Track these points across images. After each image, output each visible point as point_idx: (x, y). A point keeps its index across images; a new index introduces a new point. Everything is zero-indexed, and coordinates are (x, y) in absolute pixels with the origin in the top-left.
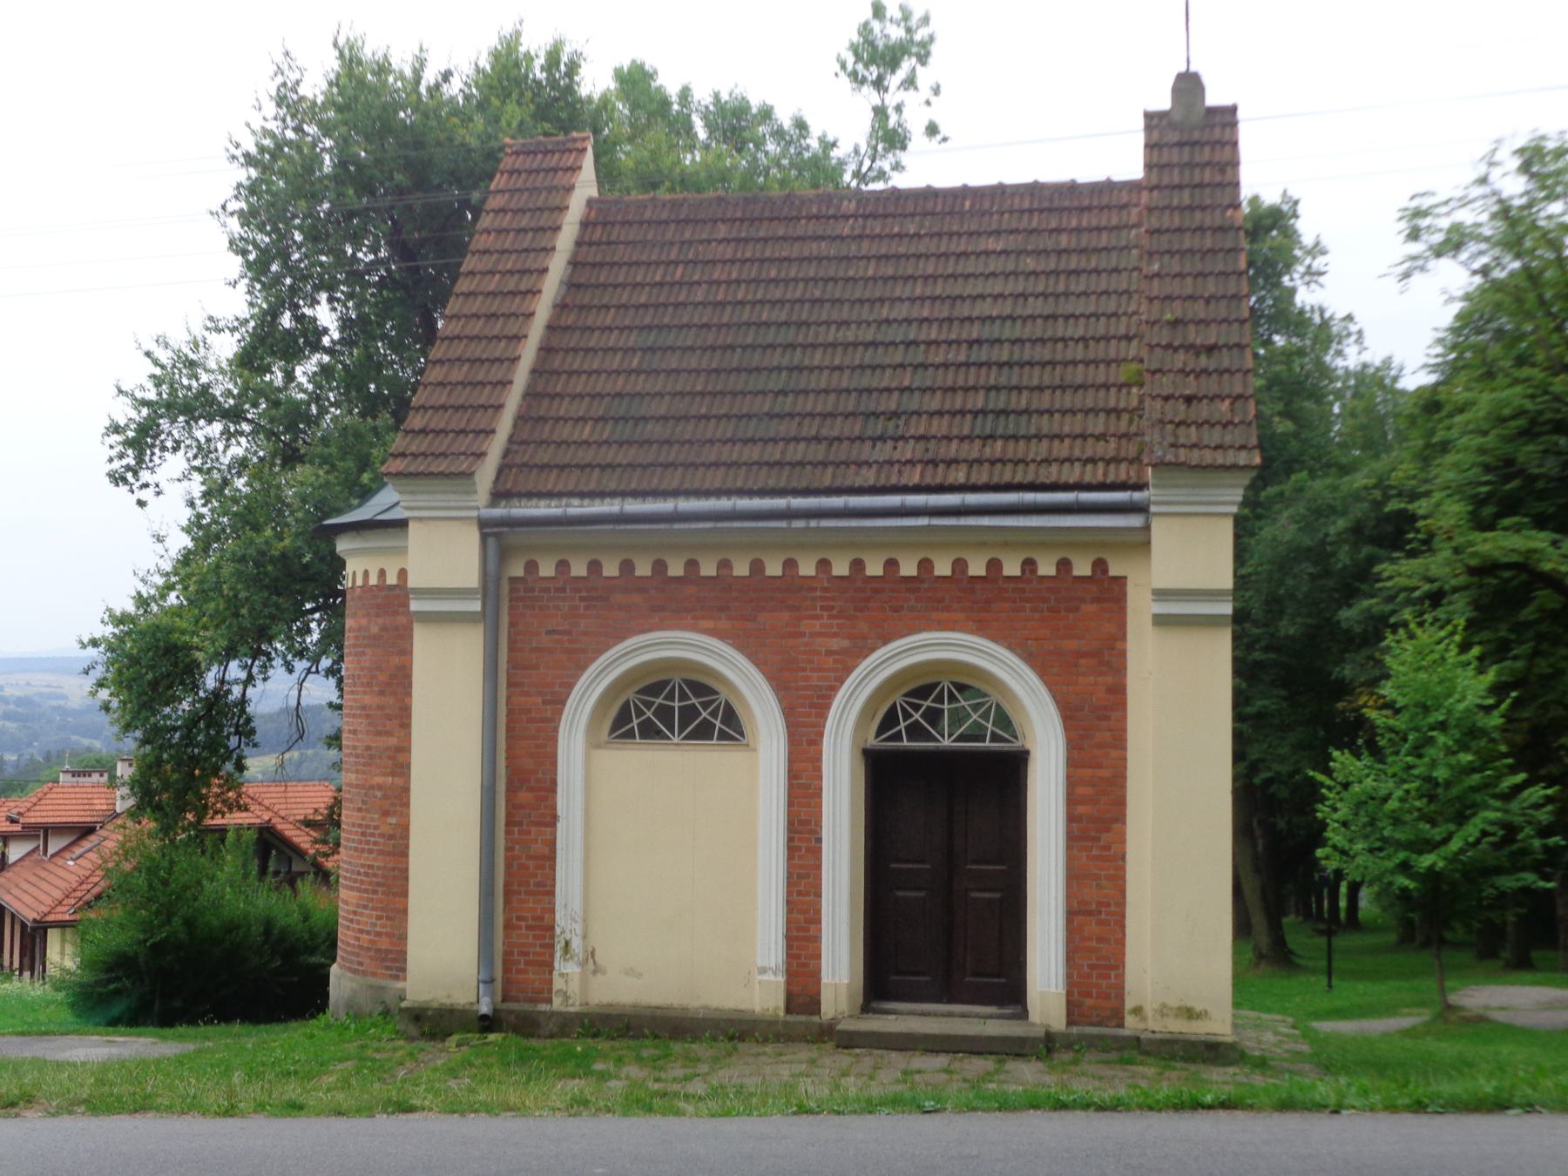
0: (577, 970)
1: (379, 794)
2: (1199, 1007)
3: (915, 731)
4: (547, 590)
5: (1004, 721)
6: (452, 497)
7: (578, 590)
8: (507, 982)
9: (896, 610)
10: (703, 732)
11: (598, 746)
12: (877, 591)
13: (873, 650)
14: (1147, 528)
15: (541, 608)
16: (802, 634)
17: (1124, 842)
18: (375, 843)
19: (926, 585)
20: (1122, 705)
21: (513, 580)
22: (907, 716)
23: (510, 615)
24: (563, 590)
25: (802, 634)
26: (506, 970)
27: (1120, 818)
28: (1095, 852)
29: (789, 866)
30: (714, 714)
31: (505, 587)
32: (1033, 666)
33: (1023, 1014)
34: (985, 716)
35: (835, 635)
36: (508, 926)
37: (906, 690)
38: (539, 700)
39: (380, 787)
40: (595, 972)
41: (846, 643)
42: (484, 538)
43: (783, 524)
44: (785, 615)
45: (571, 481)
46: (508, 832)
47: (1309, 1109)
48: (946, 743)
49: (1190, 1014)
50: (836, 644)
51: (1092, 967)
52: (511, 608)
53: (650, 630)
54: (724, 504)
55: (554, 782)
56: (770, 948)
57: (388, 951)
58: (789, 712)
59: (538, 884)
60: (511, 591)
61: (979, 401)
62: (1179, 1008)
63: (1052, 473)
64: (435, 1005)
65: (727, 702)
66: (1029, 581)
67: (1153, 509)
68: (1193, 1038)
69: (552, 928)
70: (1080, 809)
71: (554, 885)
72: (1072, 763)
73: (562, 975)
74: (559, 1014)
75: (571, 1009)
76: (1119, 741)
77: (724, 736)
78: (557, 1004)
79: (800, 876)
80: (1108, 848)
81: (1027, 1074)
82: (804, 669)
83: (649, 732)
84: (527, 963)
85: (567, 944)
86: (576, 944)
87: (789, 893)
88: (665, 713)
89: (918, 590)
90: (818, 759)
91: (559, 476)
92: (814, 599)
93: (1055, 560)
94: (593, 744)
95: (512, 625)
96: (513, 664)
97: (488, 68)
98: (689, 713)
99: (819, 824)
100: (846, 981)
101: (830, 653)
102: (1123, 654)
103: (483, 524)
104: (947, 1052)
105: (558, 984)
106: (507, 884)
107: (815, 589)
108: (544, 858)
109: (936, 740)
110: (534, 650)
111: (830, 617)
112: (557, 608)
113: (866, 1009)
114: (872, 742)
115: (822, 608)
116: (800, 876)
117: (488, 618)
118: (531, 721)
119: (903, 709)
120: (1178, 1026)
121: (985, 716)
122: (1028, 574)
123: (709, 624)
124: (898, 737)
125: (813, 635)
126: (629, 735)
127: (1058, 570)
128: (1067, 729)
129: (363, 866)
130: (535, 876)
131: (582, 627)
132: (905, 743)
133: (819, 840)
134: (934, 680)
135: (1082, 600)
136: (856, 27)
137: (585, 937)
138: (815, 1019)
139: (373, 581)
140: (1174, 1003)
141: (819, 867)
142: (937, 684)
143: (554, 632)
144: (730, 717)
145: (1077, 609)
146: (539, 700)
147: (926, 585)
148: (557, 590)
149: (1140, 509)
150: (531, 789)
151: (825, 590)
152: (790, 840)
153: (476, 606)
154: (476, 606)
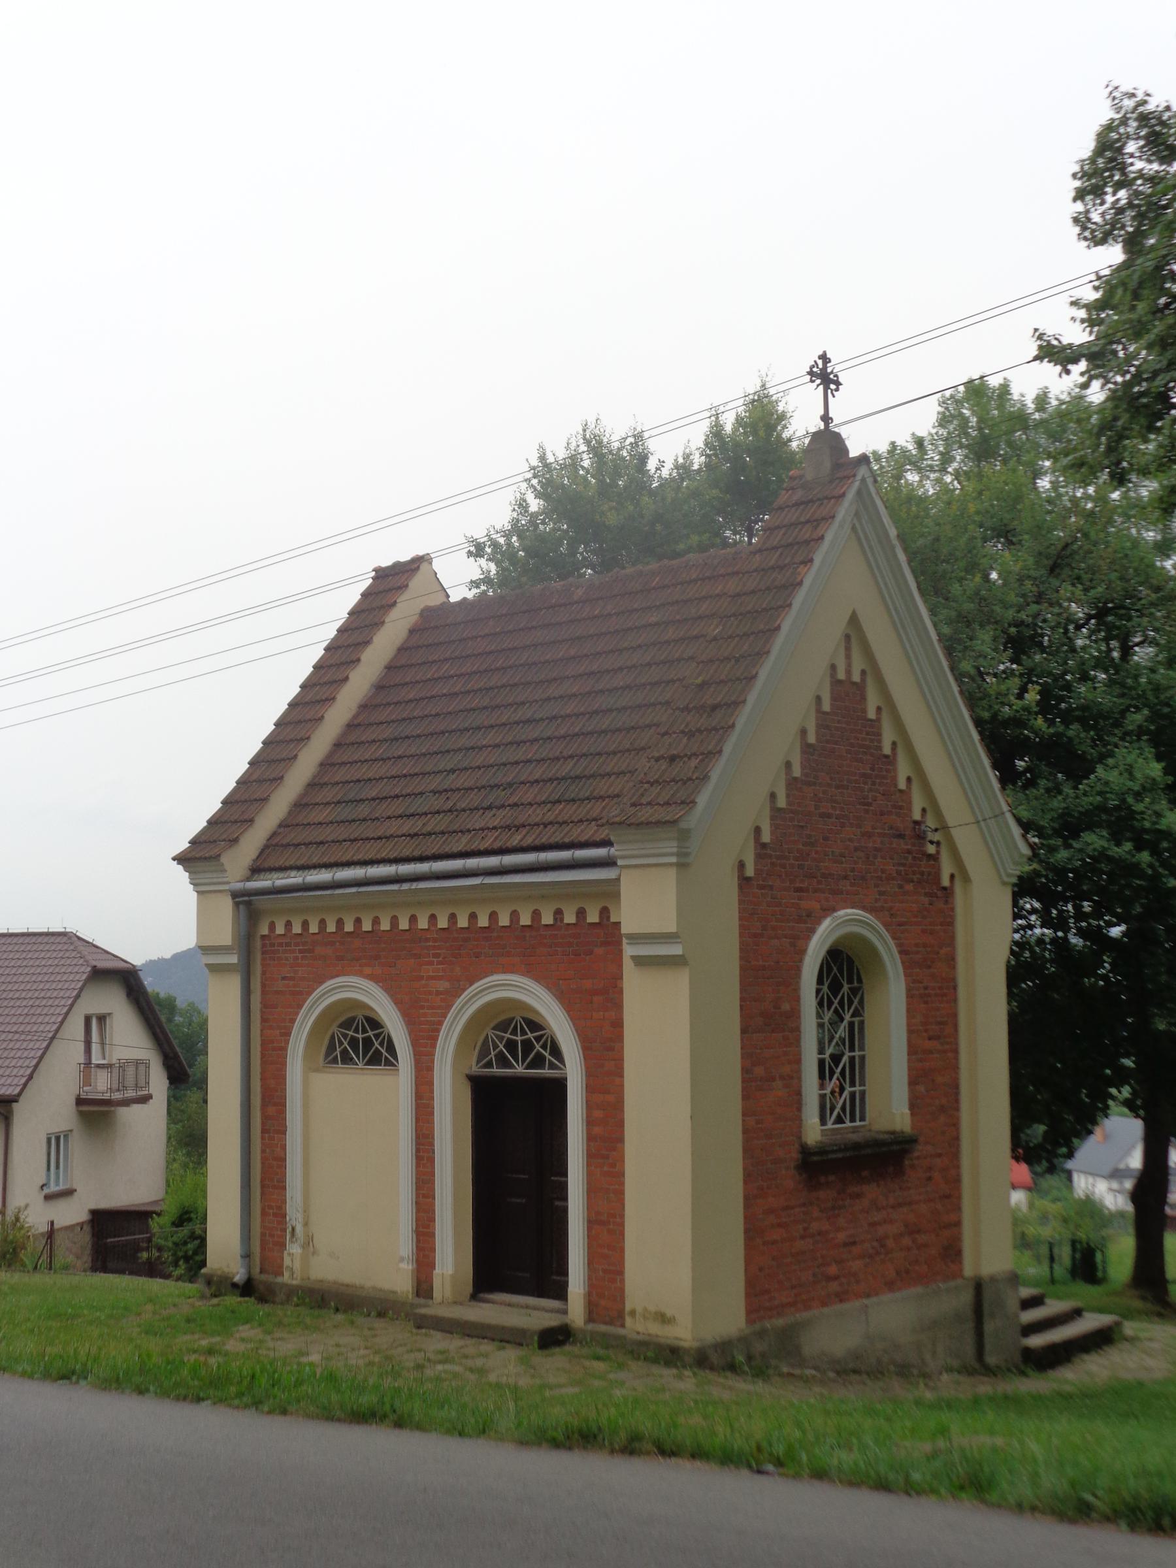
0: (300, 1251)
2: (669, 1313)
4: (281, 945)
6: (215, 875)
8: (263, 1259)
9: (477, 956)
11: (317, 1070)
13: (464, 990)
14: (618, 880)
16: (421, 978)
19: (495, 934)
20: (620, 1037)
21: (263, 937)
22: (538, 1039)
23: (262, 964)
25: (421, 978)
26: (263, 1248)
27: (621, 1140)
28: (606, 1169)
29: (417, 1172)
30: (523, 1033)
31: (258, 943)
35: (440, 978)
36: (264, 1213)
37: (492, 1025)
38: (278, 1032)
40: (314, 1253)
42: (237, 905)
43: (395, 887)
46: (263, 1138)
49: (663, 1318)
50: (443, 985)
51: (605, 1271)
52: (263, 959)
53: (337, 976)
54: (358, 872)
60: (264, 946)
62: (656, 1313)
63: (576, 834)
64: (219, 1273)
67: (620, 862)
68: (662, 1341)
69: (284, 1216)
70: (597, 1130)
73: (289, 1254)
74: (286, 1285)
75: (294, 1282)
78: (286, 1278)
83: (346, 1059)
85: (293, 1229)
86: (299, 1229)
87: (417, 1196)
90: (431, 1084)
91: (316, 849)
93: (599, 907)
94: (310, 1067)
95: (264, 973)
96: (265, 1005)
97: (728, 428)
100: (450, 1272)
101: (438, 993)
103: (235, 895)
104: (478, 1337)
105: (287, 1261)
106: (262, 1180)
107: (427, 940)
109: (514, 1067)
111: (439, 963)
112: (287, 959)
113: (474, 1297)
114: (476, 1070)
117: (620, 936)
120: (655, 1329)
122: (559, 923)
123: (368, 970)
124: (489, 1065)
126: (335, 1061)
127: (577, 917)
132: (495, 1070)
134: (512, 1016)
137: (306, 1224)
140: (652, 1308)
141: (433, 1175)
142: (334, 1033)
145: (591, 952)
146: (278, 1032)
147: (495, 934)
149: (609, 863)
151: (435, 940)
152: (418, 1150)
153: (233, 959)
154: (233, 959)
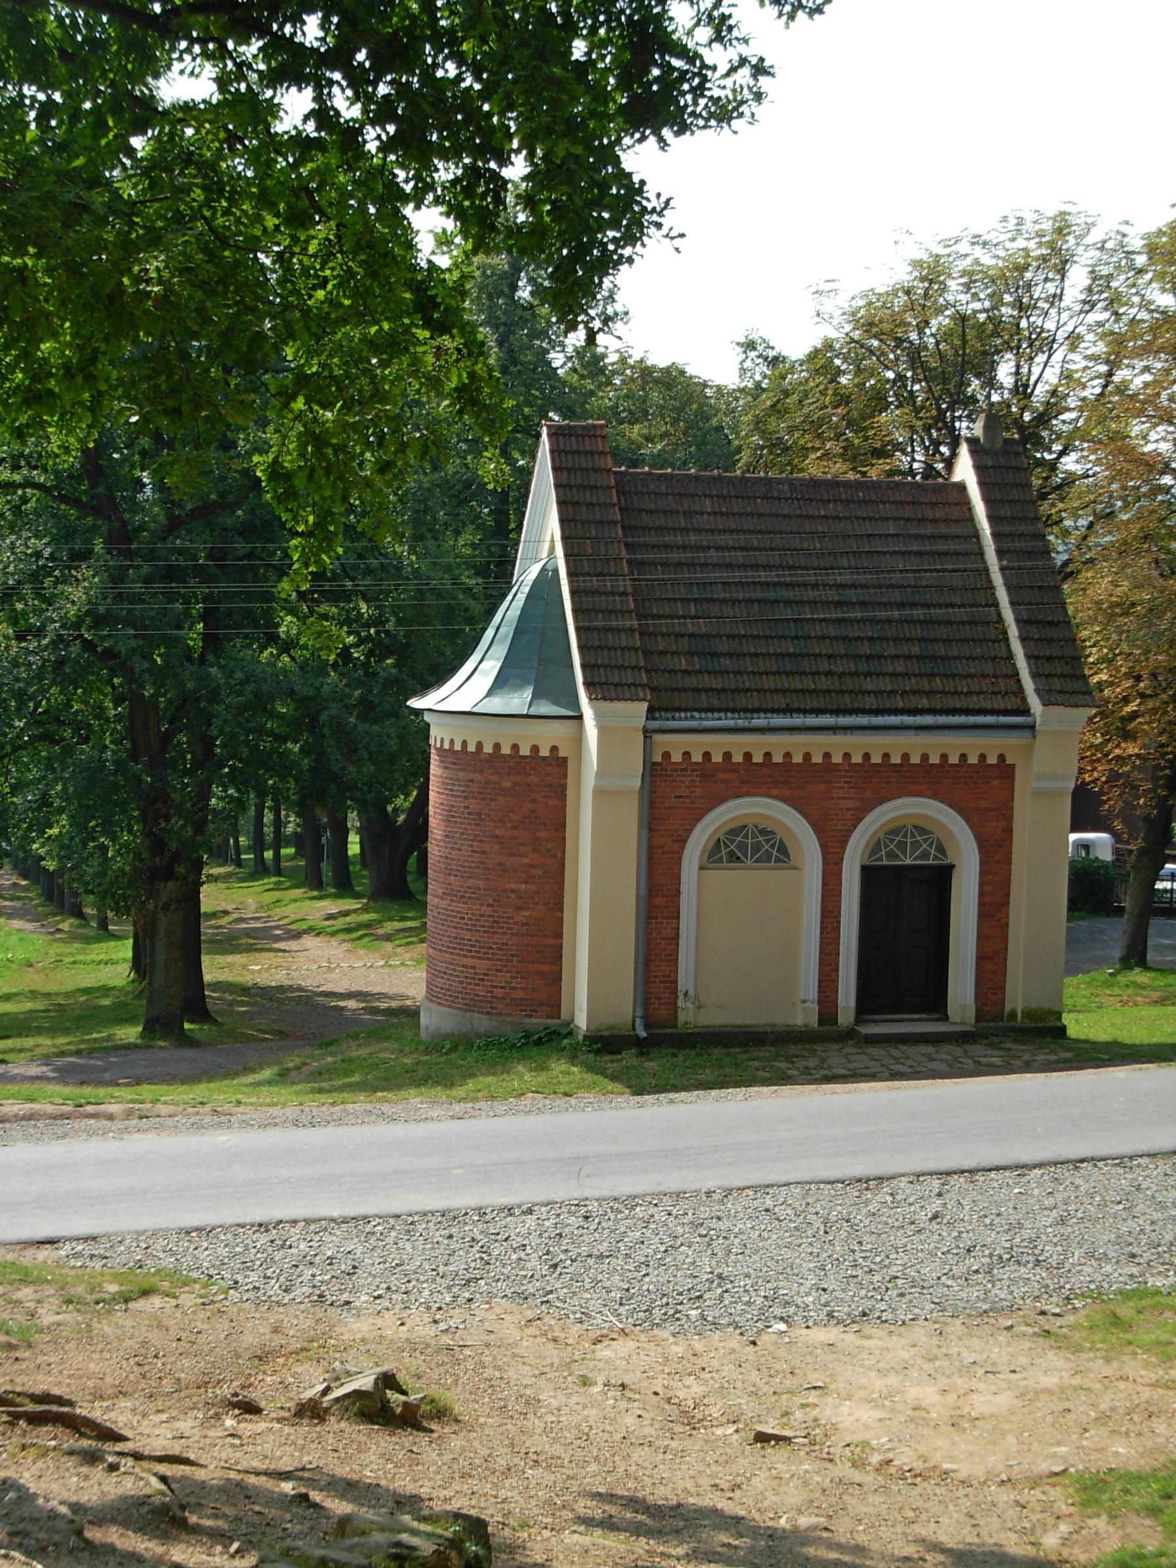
1: (513, 896)
3: (891, 855)
5: (941, 850)
7: (695, 770)
10: (767, 858)
12: (879, 772)
15: (671, 782)
17: (1008, 917)
18: (509, 928)
22: (886, 846)
24: (685, 770)
27: (1006, 904)
32: (963, 817)
33: (945, 1018)
34: (931, 845)
35: (852, 798)
39: (513, 891)
41: (857, 804)
44: (823, 786)
45: (755, 701)
47: (877, 1042)
48: (908, 862)
50: (852, 804)
55: (678, 891)
56: (809, 989)
57: (522, 999)
58: (824, 847)
59: (667, 955)
61: (916, 650)
63: (974, 702)
65: (781, 840)
66: (962, 766)
70: (986, 899)
71: (677, 955)
72: (983, 872)
76: (1008, 860)
77: (778, 860)
79: (828, 944)
80: (999, 920)
81: (949, 1051)
82: (833, 820)
83: (733, 858)
84: (660, 1004)
88: (742, 847)
89: (899, 771)
90: (839, 873)
92: (840, 777)
98: (757, 848)
99: (839, 912)
101: (848, 809)
102: (1012, 809)
108: (672, 939)
110: (667, 808)
112: (682, 781)
115: (845, 782)
116: (828, 944)
118: (664, 853)
119: (885, 842)
121: (931, 845)
125: (840, 798)
126: (720, 860)
128: (980, 853)
129: (494, 943)
130: (665, 950)
131: (698, 794)
132: (885, 863)
133: (839, 922)
135: (990, 777)
136: (680, 361)
138: (835, 1028)
139: (458, 747)
141: (839, 938)
143: (680, 797)
144: (783, 849)
148: (682, 770)
150: (663, 896)
151: (846, 771)
